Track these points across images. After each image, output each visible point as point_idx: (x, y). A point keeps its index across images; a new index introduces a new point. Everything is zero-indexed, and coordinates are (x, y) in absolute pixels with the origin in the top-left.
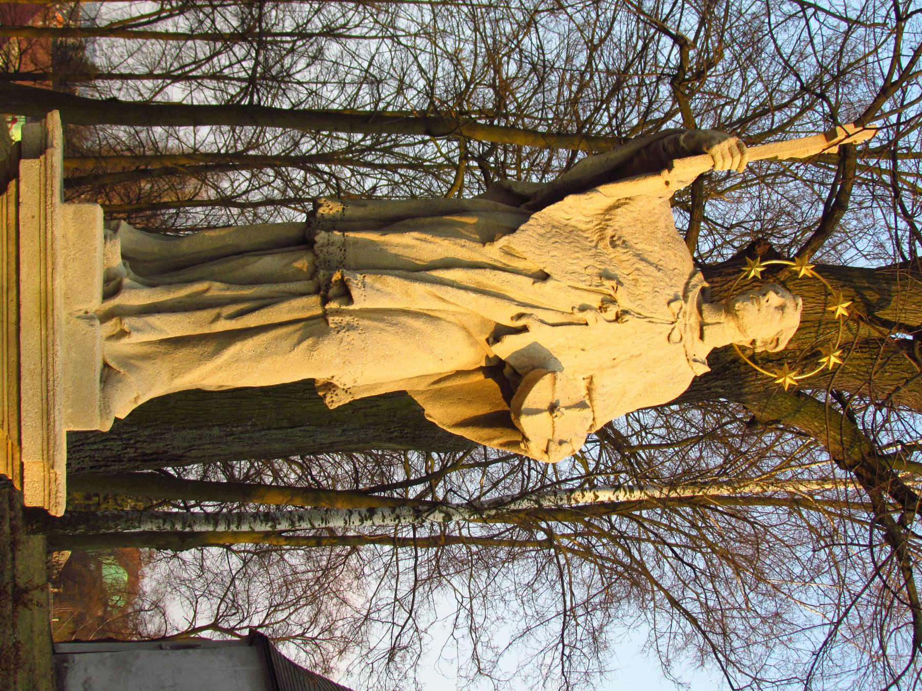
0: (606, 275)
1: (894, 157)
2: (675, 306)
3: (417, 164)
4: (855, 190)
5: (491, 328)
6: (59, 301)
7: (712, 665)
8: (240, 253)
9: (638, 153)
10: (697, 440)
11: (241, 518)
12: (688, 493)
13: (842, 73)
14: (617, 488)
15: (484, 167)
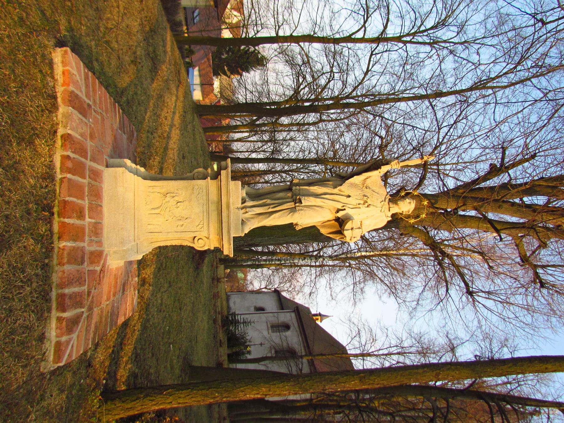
0: (365, 196)
1: (438, 165)
2: (382, 203)
3: (314, 172)
4: (428, 174)
5: (336, 210)
6: (231, 205)
7: (392, 297)
8: (274, 192)
9: (372, 165)
10: (387, 239)
11: (272, 260)
12: (385, 253)
13: (424, 144)
14: (367, 251)
15: (331, 172)
